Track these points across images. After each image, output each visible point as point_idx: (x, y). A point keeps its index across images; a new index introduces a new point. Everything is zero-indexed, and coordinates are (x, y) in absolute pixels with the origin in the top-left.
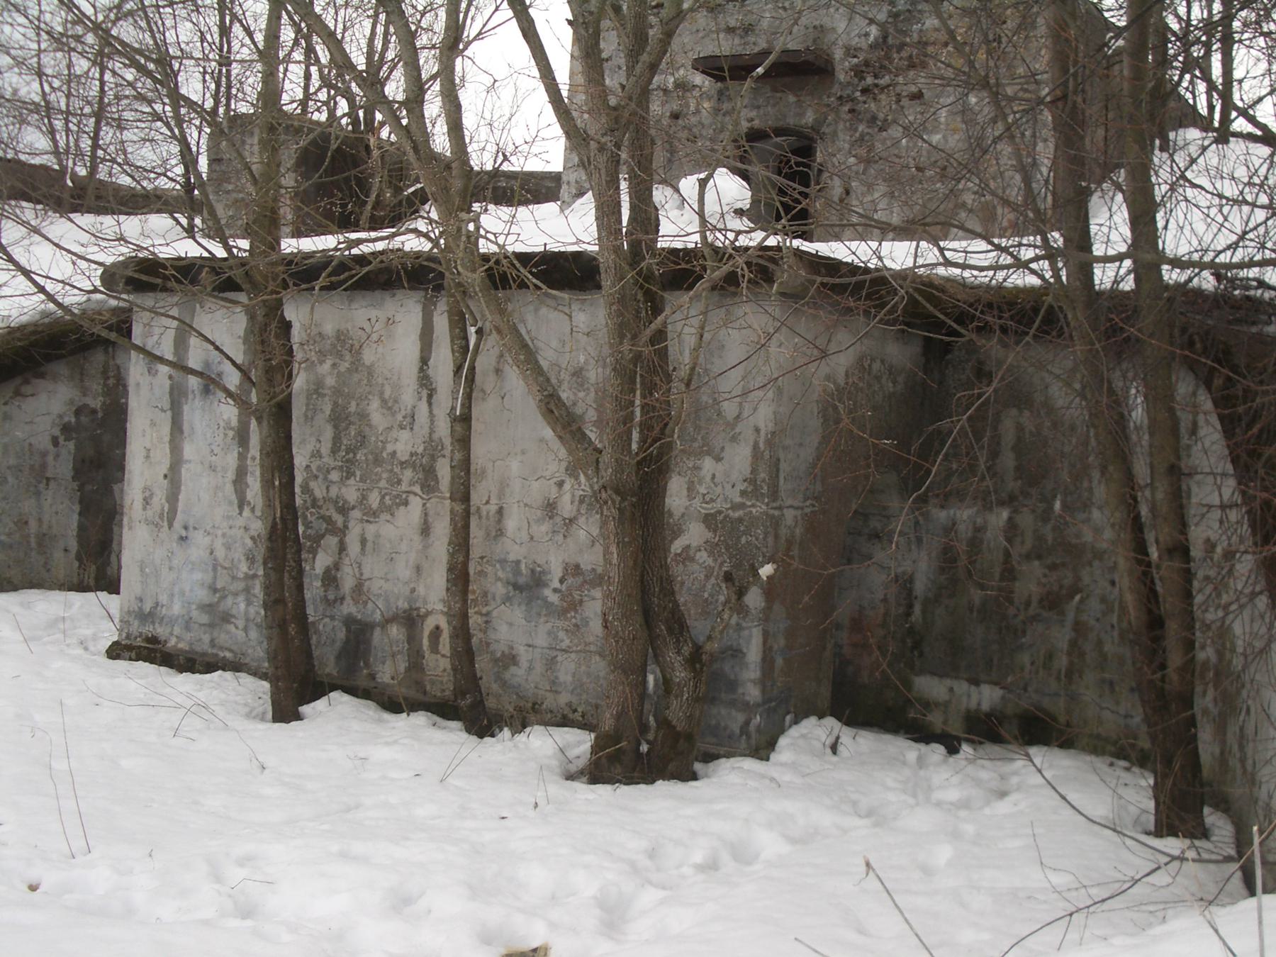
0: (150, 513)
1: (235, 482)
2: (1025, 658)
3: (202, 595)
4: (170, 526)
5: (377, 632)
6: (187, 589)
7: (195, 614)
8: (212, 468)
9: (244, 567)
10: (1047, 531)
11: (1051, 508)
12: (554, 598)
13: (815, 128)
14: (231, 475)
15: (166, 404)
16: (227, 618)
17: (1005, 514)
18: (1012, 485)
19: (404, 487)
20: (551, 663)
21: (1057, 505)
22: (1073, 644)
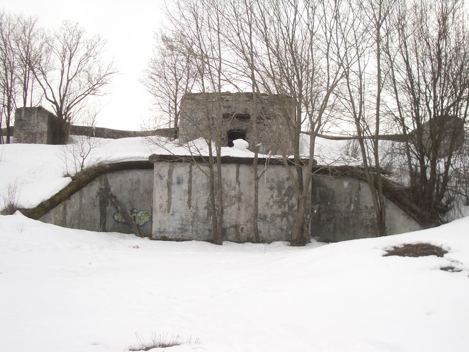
0: (162, 210)
1: (188, 202)
2: (324, 231)
3: (179, 226)
4: (168, 212)
5: (228, 230)
6: (174, 225)
7: (177, 230)
8: (181, 199)
9: (191, 219)
10: (327, 208)
11: (327, 204)
12: (269, 220)
13: (246, 130)
14: (186, 201)
15: (166, 186)
16: (186, 230)
17: (318, 205)
18: (319, 200)
19: (233, 201)
20: (269, 231)
21: (329, 203)
22: (334, 227)
